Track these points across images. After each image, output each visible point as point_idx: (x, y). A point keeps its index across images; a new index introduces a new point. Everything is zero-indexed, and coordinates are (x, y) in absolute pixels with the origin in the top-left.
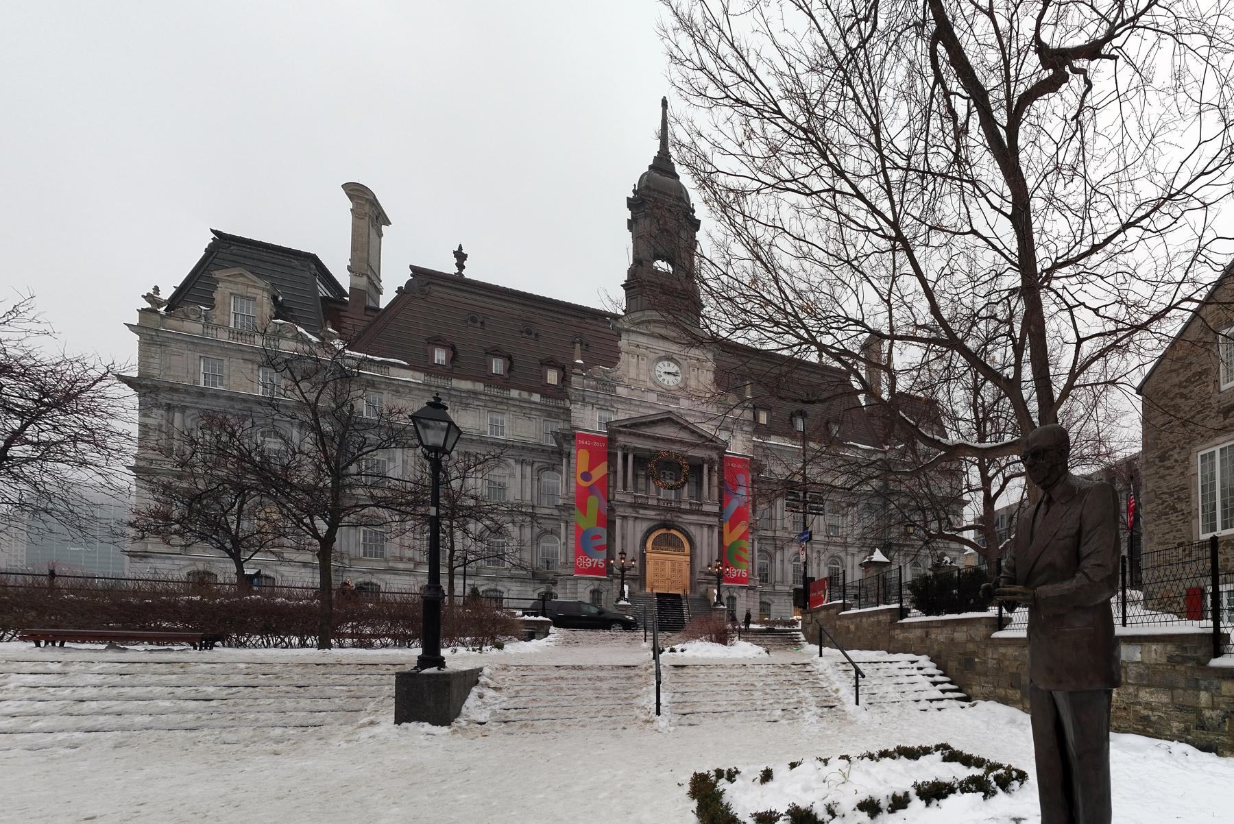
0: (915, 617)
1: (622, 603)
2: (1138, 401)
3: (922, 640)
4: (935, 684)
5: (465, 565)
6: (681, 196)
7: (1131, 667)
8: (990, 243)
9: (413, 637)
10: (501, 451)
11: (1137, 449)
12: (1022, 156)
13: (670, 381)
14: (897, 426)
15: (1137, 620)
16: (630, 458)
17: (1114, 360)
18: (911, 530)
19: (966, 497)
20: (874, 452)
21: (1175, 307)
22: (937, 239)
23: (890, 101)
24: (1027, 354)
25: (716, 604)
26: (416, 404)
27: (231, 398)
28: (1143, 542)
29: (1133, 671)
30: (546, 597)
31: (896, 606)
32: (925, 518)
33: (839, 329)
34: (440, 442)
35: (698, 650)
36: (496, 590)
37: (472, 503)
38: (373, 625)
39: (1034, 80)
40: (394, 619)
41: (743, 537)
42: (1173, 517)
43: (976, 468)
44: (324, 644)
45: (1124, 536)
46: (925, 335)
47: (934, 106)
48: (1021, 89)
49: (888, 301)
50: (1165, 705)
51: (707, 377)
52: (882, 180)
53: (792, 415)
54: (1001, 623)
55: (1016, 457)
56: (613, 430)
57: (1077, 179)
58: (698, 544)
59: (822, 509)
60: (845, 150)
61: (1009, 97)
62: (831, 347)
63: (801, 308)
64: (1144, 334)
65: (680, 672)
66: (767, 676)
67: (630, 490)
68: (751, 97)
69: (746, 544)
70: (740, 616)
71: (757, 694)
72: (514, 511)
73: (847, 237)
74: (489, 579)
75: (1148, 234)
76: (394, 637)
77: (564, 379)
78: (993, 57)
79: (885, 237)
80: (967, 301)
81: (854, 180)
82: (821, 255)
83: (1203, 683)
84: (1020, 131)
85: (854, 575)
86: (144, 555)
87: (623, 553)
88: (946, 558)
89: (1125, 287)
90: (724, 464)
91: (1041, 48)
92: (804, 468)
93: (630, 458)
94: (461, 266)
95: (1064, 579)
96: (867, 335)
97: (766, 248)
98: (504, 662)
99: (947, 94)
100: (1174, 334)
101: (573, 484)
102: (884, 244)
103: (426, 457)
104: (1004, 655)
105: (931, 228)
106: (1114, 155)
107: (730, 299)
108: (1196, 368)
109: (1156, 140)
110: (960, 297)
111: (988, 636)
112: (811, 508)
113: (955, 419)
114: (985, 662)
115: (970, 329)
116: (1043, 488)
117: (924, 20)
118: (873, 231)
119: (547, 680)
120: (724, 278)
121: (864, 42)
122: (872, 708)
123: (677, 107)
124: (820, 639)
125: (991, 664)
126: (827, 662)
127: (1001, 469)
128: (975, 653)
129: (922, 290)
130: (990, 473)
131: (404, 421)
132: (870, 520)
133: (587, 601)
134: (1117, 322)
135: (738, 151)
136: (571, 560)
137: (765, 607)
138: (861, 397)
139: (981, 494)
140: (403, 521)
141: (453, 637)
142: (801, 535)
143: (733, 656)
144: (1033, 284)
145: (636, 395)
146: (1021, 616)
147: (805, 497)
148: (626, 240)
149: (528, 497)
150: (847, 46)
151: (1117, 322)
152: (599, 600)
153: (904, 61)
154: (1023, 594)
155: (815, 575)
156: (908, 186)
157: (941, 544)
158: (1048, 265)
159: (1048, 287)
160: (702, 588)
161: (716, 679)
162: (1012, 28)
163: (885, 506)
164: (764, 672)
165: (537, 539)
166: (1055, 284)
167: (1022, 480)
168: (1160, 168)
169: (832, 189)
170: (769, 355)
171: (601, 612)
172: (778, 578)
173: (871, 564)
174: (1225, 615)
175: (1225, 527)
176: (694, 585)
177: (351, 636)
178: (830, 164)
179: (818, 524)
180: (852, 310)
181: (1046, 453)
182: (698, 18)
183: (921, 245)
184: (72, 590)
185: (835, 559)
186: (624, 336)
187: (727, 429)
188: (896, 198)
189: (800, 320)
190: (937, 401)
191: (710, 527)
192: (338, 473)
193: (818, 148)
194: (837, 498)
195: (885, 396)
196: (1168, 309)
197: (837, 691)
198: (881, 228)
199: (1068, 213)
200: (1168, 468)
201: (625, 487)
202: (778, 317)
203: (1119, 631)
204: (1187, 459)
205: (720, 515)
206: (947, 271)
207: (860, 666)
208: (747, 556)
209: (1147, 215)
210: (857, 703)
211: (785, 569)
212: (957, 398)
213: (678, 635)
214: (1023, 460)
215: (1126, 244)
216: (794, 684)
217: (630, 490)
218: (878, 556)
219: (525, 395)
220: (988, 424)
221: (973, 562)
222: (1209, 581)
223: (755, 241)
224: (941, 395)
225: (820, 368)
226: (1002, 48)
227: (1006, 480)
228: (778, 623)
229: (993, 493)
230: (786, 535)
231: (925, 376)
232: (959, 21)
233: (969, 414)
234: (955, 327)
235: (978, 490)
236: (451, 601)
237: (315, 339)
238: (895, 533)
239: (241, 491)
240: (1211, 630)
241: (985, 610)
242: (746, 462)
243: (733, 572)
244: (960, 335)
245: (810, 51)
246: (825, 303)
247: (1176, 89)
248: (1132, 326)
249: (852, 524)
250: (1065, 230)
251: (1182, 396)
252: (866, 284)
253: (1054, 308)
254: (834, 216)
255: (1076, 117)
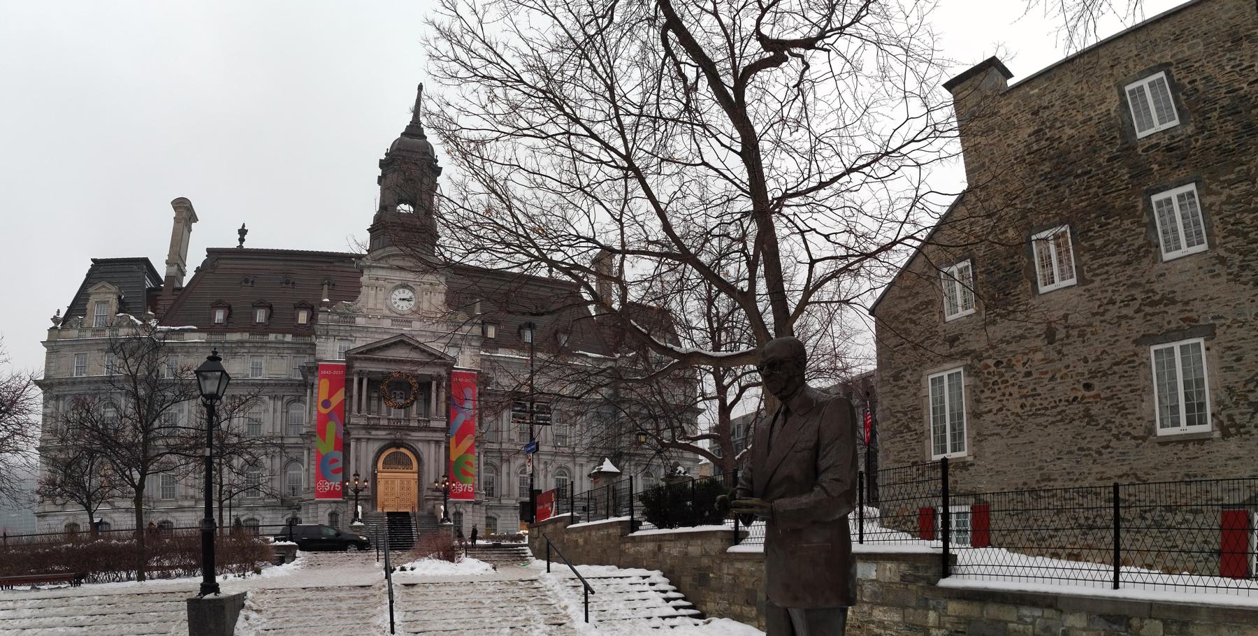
0: (648, 529)
1: (357, 523)
2: (871, 322)
3: (655, 554)
4: (668, 600)
5: (230, 498)
6: (428, 151)
7: (867, 585)
8: (721, 174)
9: (195, 567)
10: (258, 389)
11: (872, 366)
12: (748, 109)
13: (405, 307)
14: (628, 334)
15: (875, 537)
16: (365, 382)
17: (846, 282)
18: (643, 438)
19: (701, 405)
20: (605, 360)
21: (900, 242)
22: (668, 169)
23: (624, 68)
24: (761, 270)
25: (443, 520)
26: (198, 361)
27: (89, 381)
28: (879, 459)
29: (868, 589)
30: (293, 522)
31: (627, 518)
32: (657, 426)
33: (570, 246)
34: (215, 390)
35: (426, 568)
36: (253, 519)
37: (235, 440)
38: (169, 558)
39: (757, 58)
40: (183, 551)
41: (470, 450)
42: (907, 436)
43: (711, 376)
44: (141, 578)
45: (862, 451)
46: (657, 249)
47: (666, 71)
48: (746, 63)
49: (620, 221)
50: (896, 623)
51: (439, 299)
52: (615, 123)
53: (521, 328)
54: (737, 537)
55: (752, 367)
56: (351, 358)
57: (801, 130)
58: (426, 461)
59: (549, 419)
60: (580, 103)
61: (734, 67)
62: (562, 262)
63: (533, 230)
64: (874, 262)
65: (410, 590)
66: (494, 593)
67: (364, 413)
68: (495, 72)
69: (472, 458)
70: (467, 533)
71: (485, 612)
72: (267, 443)
73: (580, 169)
74: (249, 509)
75: (869, 179)
76: (184, 567)
77: (312, 318)
78: (719, 41)
79: (617, 167)
80: (699, 221)
81: (587, 124)
82: (555, 185)
83: (932, 603)
84: (746, 91)
85: (583, 486)
86: (41, 516)
87: (357, 475)
88: (680, 468)
89: (854, 219)
90: (453, 381)
91: (762, 38)
92: (531, 378)
93: (365, 382)
94: (242, 240)
95: (801, 493)
96: (598, 251)
97: (502, 183)
98: (262, 586)
99: (677, 64)
100: (901, 265)
101: (315, 413)
102: (616, 173)
103: (205, 405)
104: (740, 570)
105: (663, 160)
106: (834, 116)
107: (465, 228)
108: (922, 298)
109: (869, 110)
110: (692, 216)
111: (724, 551)
112: (538, 418)
113: (688, 327)
114: (720, 578)
115: (703, 245)
116: (781, 399)
117: (656, 17)
118: (606, 163)
119: (297, 601)
120: (460, 211)
121: (600, 31)
122: (602, 626)
123: (431, 87)
124: (547, 554)
125: (727, 579)
126: (555, 578)
127: (737, 378)
128: (709, 568)
129: (654, 210)
130: (727, 381)
131: (191, 376)
132: (599, 429)
133: (327, 523)
134: (848, 248)
135: (481, 111)
136: (312, 485)
137: (491, 522)
138: (591, 308)
139: (717, 402)
140: (187, 464)
141: (224, 565)
142: (528, 446)
143: (460, 573)
144: (764, 210)
145: (372, 323)
146: (758, 530)
147: (532, 407)
148: (376, 191)
149: (278, 429)
150: (585, 33)
151: (848, 248)
152: (337, 522)
153: (638, 42)
154: (761, 507)
155: (542, 487)
156: (640, 128)
157: (674, 453)
158: (779, 194)
159: (779, 212)
160: (430, 505)
161: (445, 597)
162: (734, 24)
163: (615, 414)
164: (491, 589)
165: (284, 468)
166: (785, 210)
167: (759, 390)
168: (876, 129)
169: (568, 133)
170: (499, 273)
171: (338, 534)
172: (504, 491)
173: (601, 474)
174: (953, 536)
175: (954, 450)
176: (421, 502)
177: (157, 569)
178: (566, 114)
179: (545, 434)
180: (583, 228)
181: (783, 365)
182: (456, 28)
183: (653, 173)
184: (14, 546)
185: (562, 470)
186: (365, 272)
187: (455, 346)
188: (629, 137)
189: (531, 241)
190: (670, 311)
191: (437, 442)
192: (147, 430)
193: (556, 103)
194: (565, 407)
195: (616, 306)
196: (894, 243)
197: (566, 608)
198: (614, 160)
199: (795, 155)
200: (902, 388)
201: (359, 410)
202: (510, 239)
203: (856, 548)
204: (919, 381)
205: (446, 430)
206: (679, 195)
207: (589, 582)
208: (473, 470)
209: (868, 165)
210: (587, 621)
211: (511, 482)
212: (691, 308)
213: (407, 554)
214: (759, 370)
215: (850, 186)
216: (522, 601)
217: (364, 413)
218: (608, 466)
219: (280, 337)
220: (723, 334)
221: (709, 472)
222: (940, 502)
223: (492, 178)
224: (673, 305)
225: (551, 282)
226: (727, 36)
227: (742, 390)
228: (505, 538)
229: (729, 402)
230: (513, 447)
231: (657, 286)
232: (687, 17)
233: (703, 324)
234: (688, 243)
235: (713, 398)
236: (221, 532)
237: (139, 323)
238: (625, 442)
239: (92, 454)
240: (941, 551)
241: (721, 523)
242: (473, 375)
243: (459, 487)
244: (693, 250)
245: (552, 39)
246: (556, 224)
247: (883, 78)
248: (862, 254)
249: (581, 434)
250: (792, 166)
251: (912, 321)
252: (597, 206)
253: (786, 231)
254: (568, 153)
255: (797, 85)
